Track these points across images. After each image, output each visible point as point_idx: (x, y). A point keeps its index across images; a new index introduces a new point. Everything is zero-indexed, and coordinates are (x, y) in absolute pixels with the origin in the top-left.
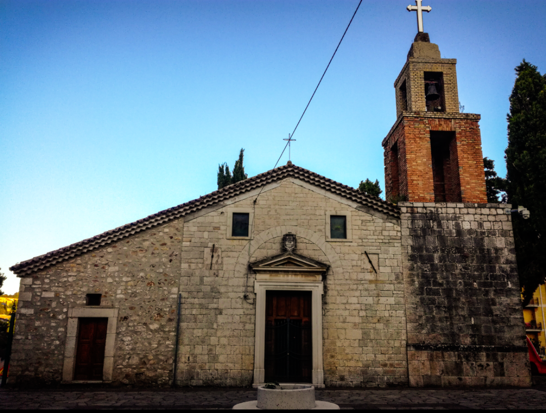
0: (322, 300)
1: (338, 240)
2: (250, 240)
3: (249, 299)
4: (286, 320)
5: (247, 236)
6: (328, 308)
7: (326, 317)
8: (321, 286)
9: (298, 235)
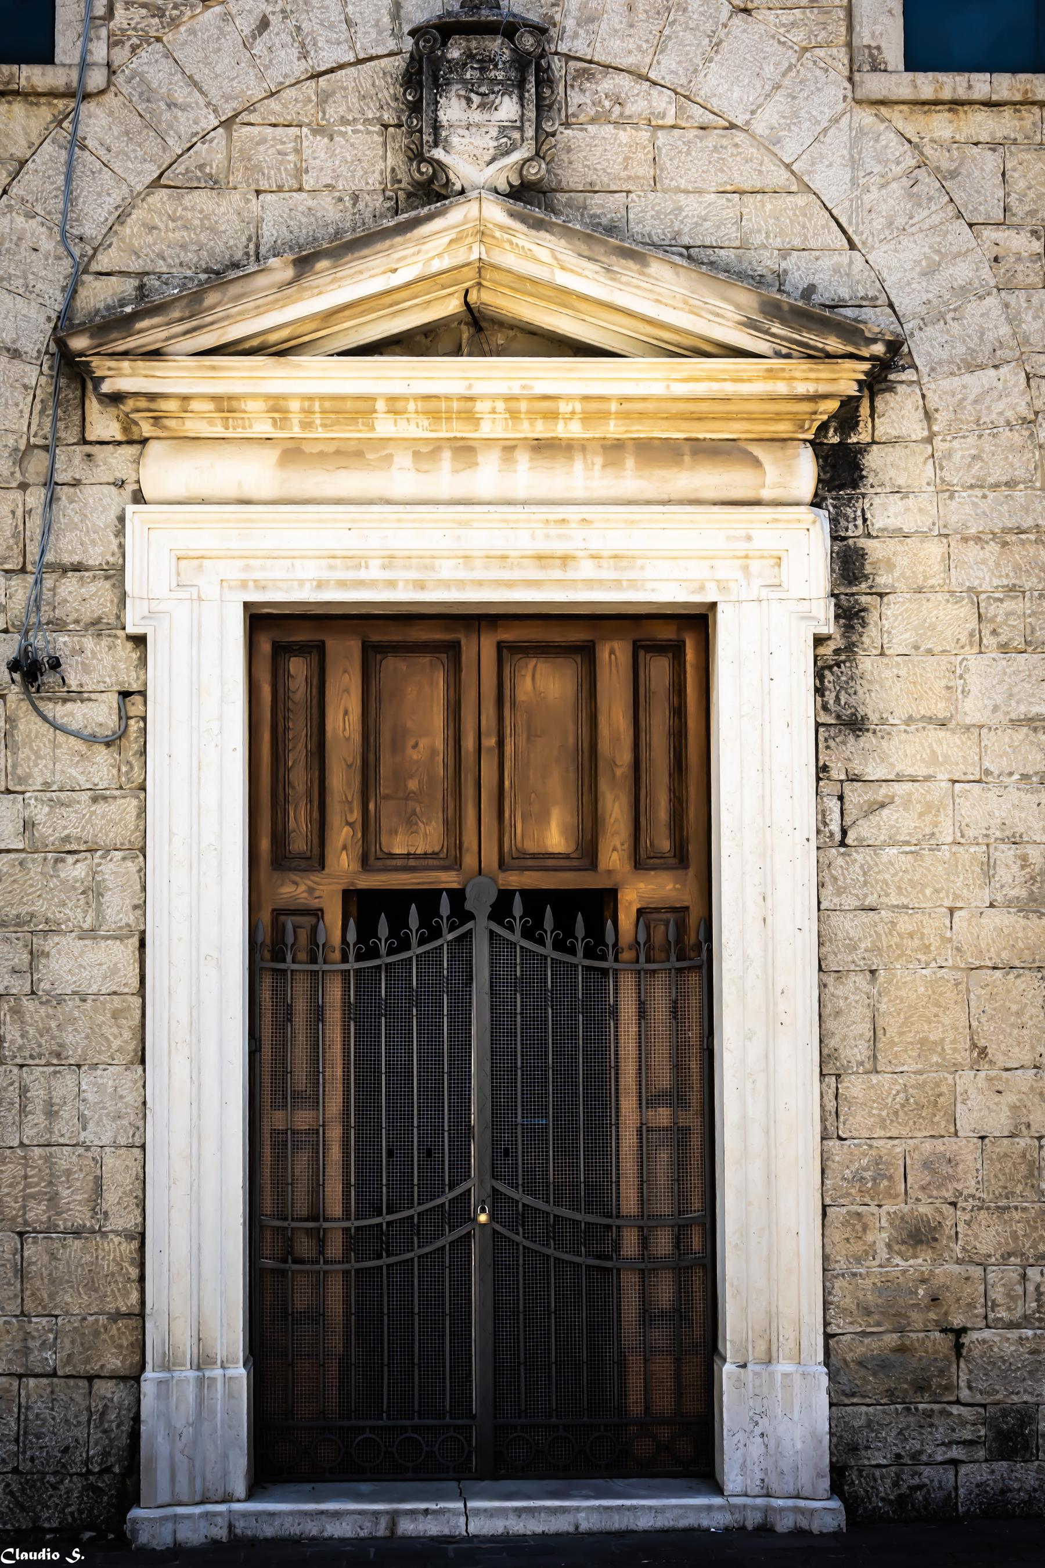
0: (819, 691)
1: (981, 85)
2: (68, 94)
3: (79, 696)
4: (457, 896)
5: (46, 56)
6: (874, 771)
7: (859, 856)
8: (805, 546)
9: (574, 41)
